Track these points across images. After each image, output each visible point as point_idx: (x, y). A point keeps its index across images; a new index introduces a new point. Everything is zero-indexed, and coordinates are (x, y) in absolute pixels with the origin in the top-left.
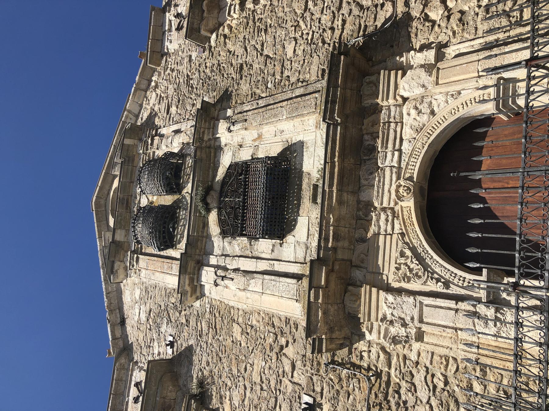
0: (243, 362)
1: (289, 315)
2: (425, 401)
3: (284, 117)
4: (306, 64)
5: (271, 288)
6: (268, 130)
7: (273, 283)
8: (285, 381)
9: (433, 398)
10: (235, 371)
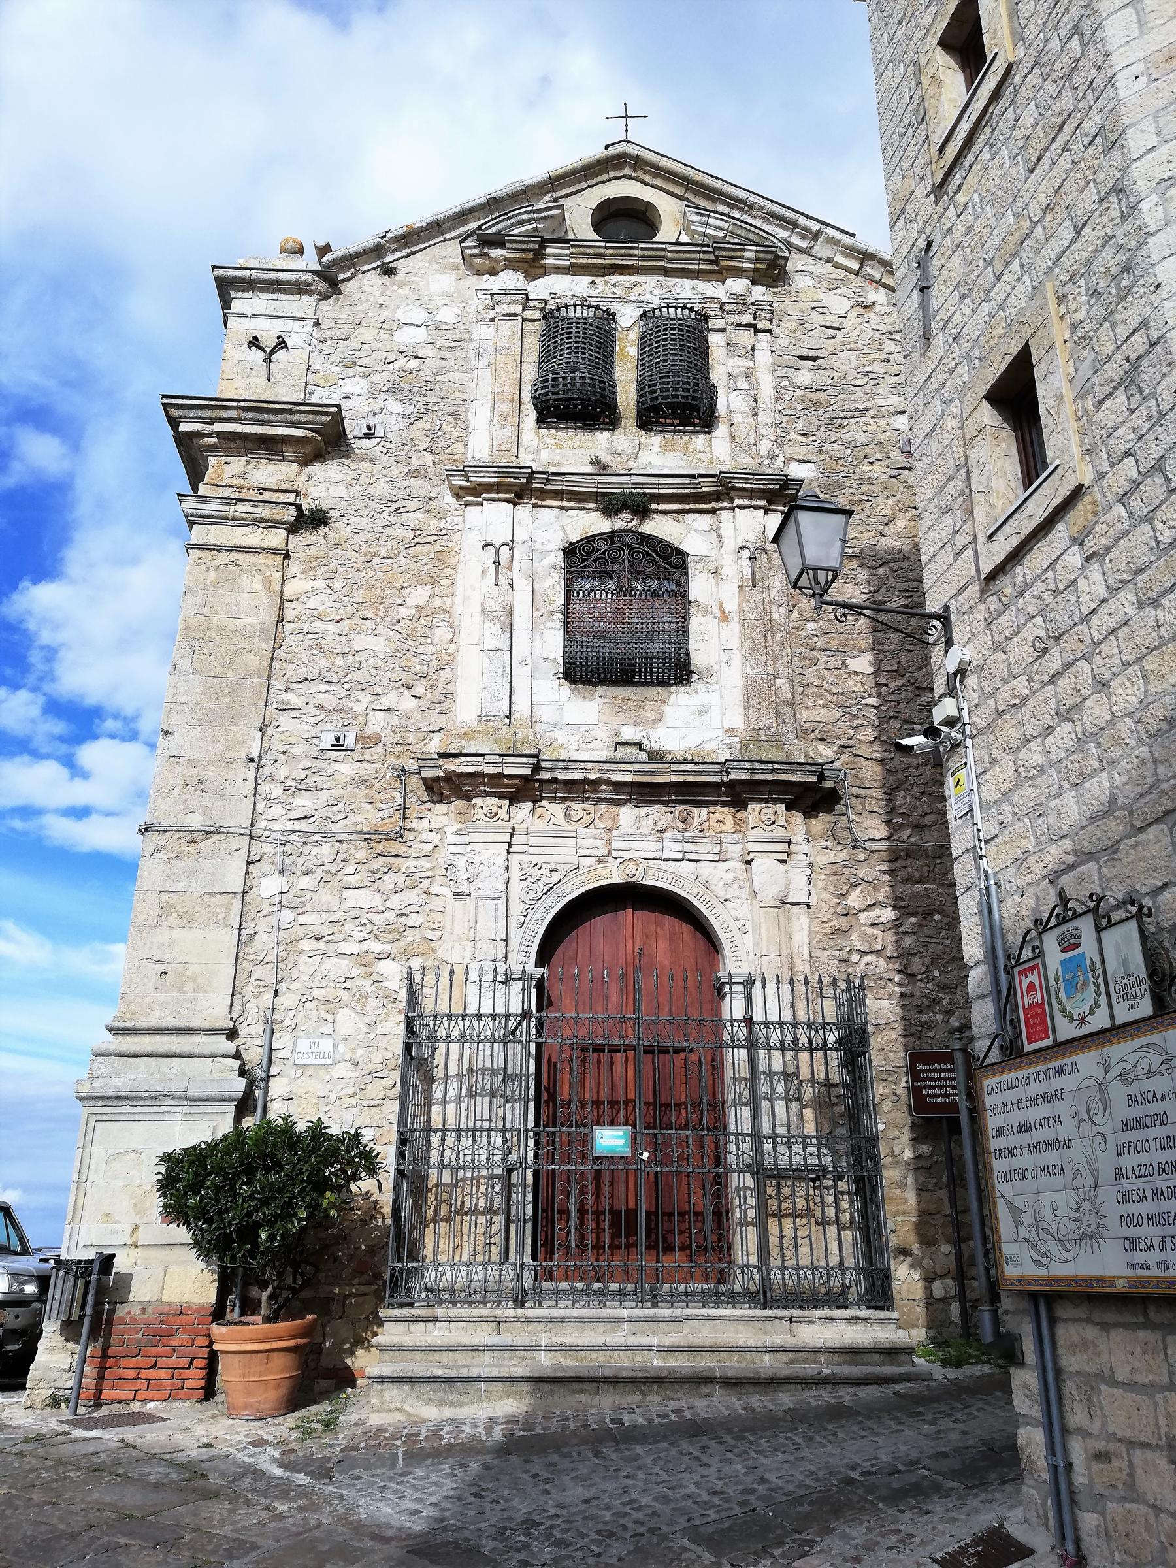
0: (376, 613)
1: (459, 699)
2: (388, 904)
3: (749, 671)
4: (830, 697)
5: (492, 668)
6: (732, 633)
7: (500, 672)
8: (366, 698)
9: (393, 914)
10: (359, 596)
